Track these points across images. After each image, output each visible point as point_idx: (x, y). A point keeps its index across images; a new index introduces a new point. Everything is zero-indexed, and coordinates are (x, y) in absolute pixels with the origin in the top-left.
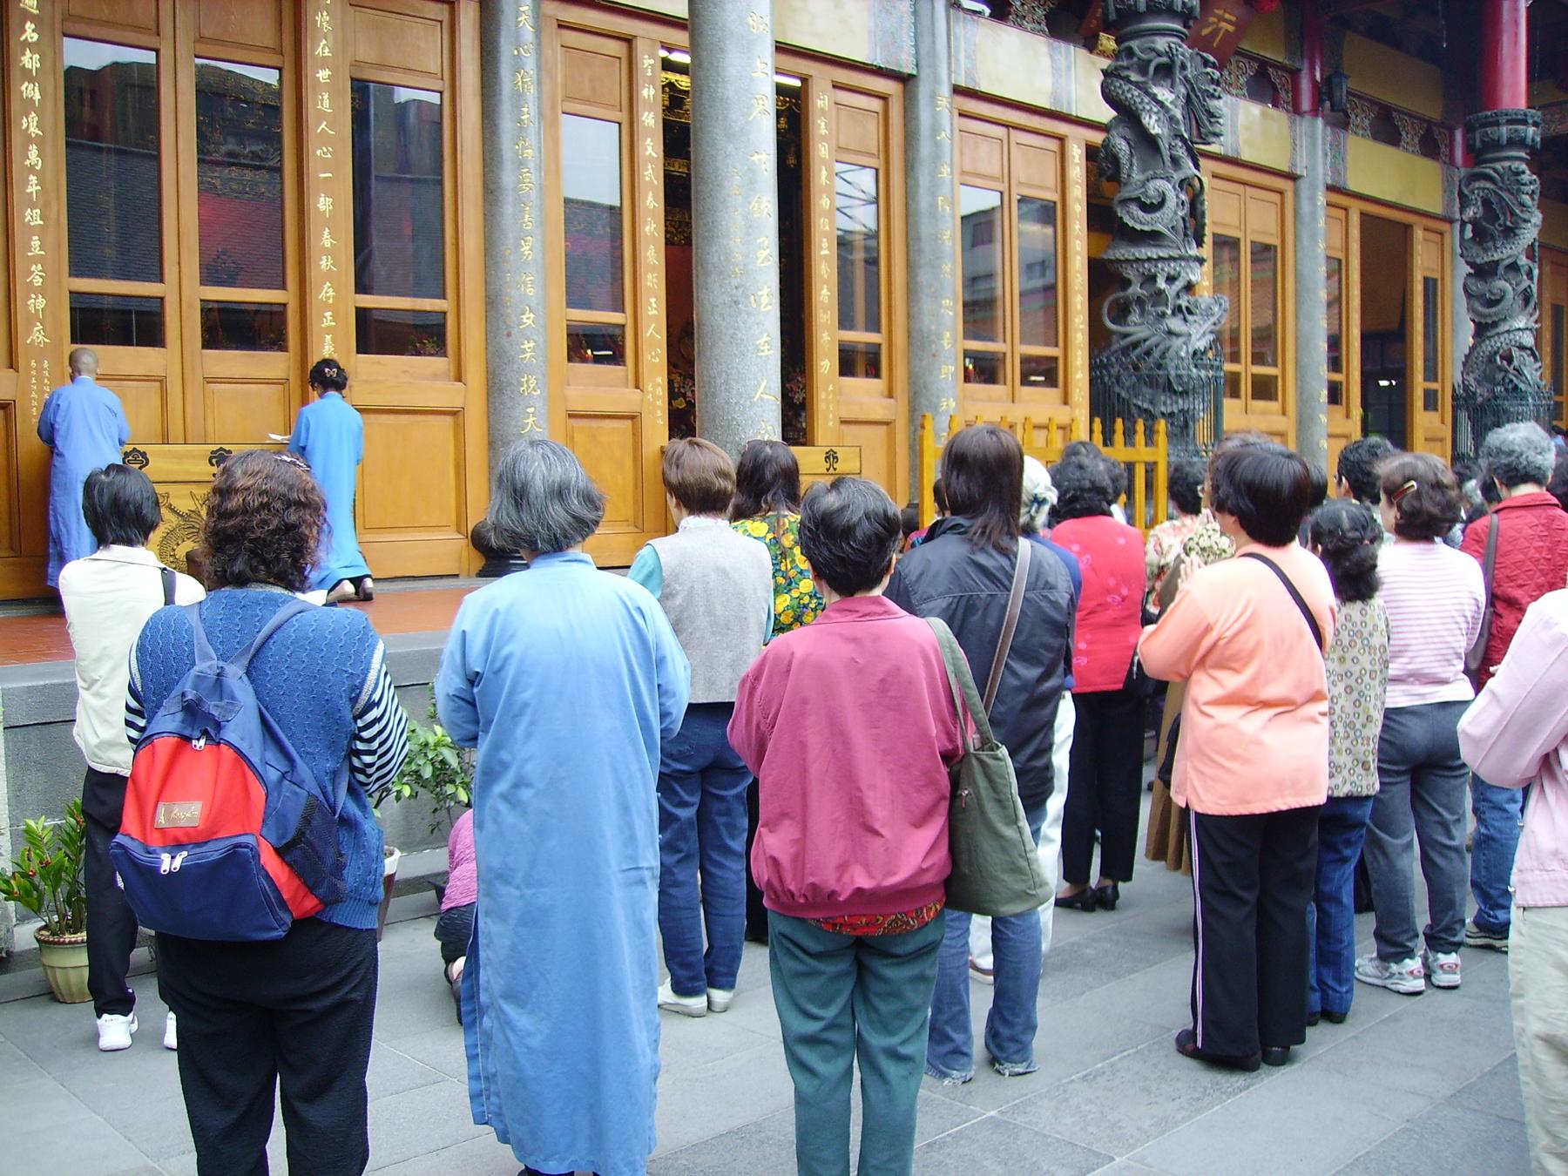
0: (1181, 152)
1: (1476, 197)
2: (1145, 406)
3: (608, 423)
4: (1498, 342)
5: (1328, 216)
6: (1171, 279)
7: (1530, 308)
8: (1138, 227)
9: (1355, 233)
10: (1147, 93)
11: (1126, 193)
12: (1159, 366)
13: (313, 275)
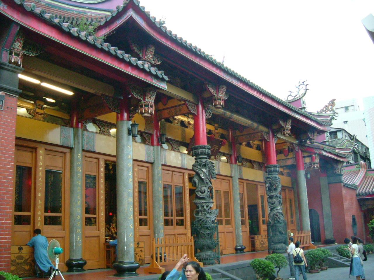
0: (208, 181)
1: (268, 182)
2: (203, 232)
3: (93, 238)
4: (274, 212)
5: (239, 184)
6: (207, 207)
7: (281, 205)
8: (200, 196)
9: (245, 187)
10: (201, 170)
11: (198, 189)
12: (205, 224)
13: (37, 210)
